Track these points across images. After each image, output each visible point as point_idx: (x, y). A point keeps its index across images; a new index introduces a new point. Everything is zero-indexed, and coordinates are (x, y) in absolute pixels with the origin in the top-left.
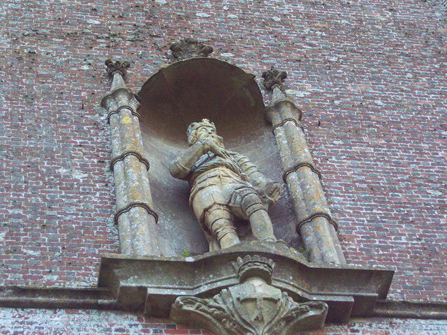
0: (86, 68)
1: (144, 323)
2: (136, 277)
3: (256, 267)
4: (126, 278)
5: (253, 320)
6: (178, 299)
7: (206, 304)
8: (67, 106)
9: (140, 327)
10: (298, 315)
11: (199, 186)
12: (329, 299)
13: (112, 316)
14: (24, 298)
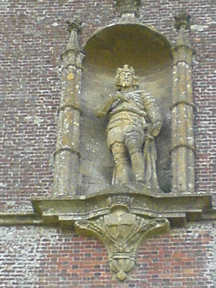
0: (56, 24)
1: (60, 234)
2: (52, 209)
3: (118, 204)
4: (46, 210)
5: (116, 237)
6: (76, 223)
8: (39, 61)
10: (148, 228)
11: (110, 127)
13: (42, 230)
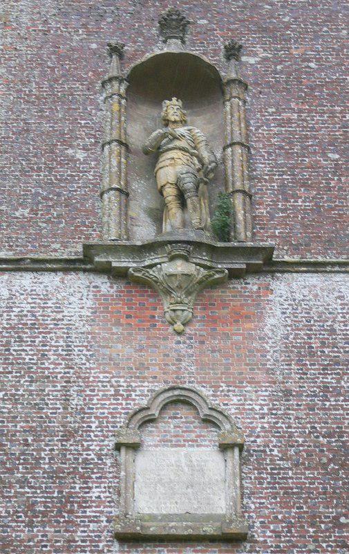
6: (131, 270)
7: (148, 272)
9: (109, 284)
12: (230, 266)
13: (92, 277)
14: (36, 266)
